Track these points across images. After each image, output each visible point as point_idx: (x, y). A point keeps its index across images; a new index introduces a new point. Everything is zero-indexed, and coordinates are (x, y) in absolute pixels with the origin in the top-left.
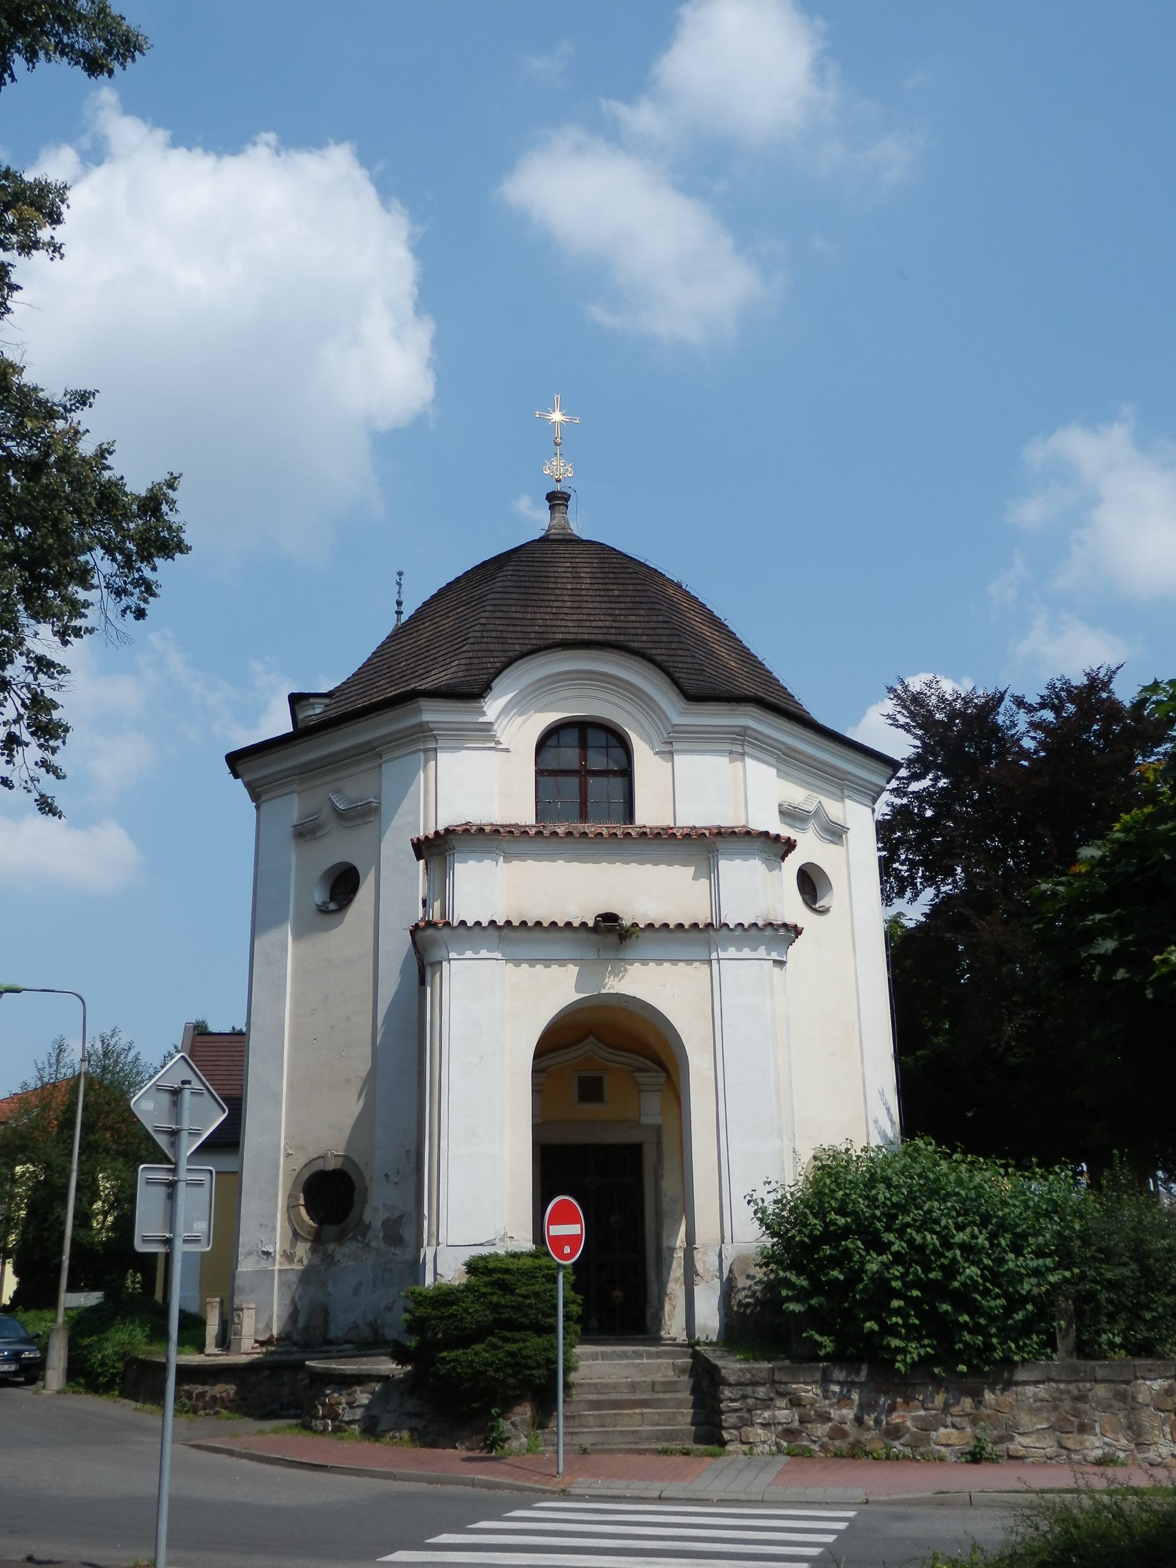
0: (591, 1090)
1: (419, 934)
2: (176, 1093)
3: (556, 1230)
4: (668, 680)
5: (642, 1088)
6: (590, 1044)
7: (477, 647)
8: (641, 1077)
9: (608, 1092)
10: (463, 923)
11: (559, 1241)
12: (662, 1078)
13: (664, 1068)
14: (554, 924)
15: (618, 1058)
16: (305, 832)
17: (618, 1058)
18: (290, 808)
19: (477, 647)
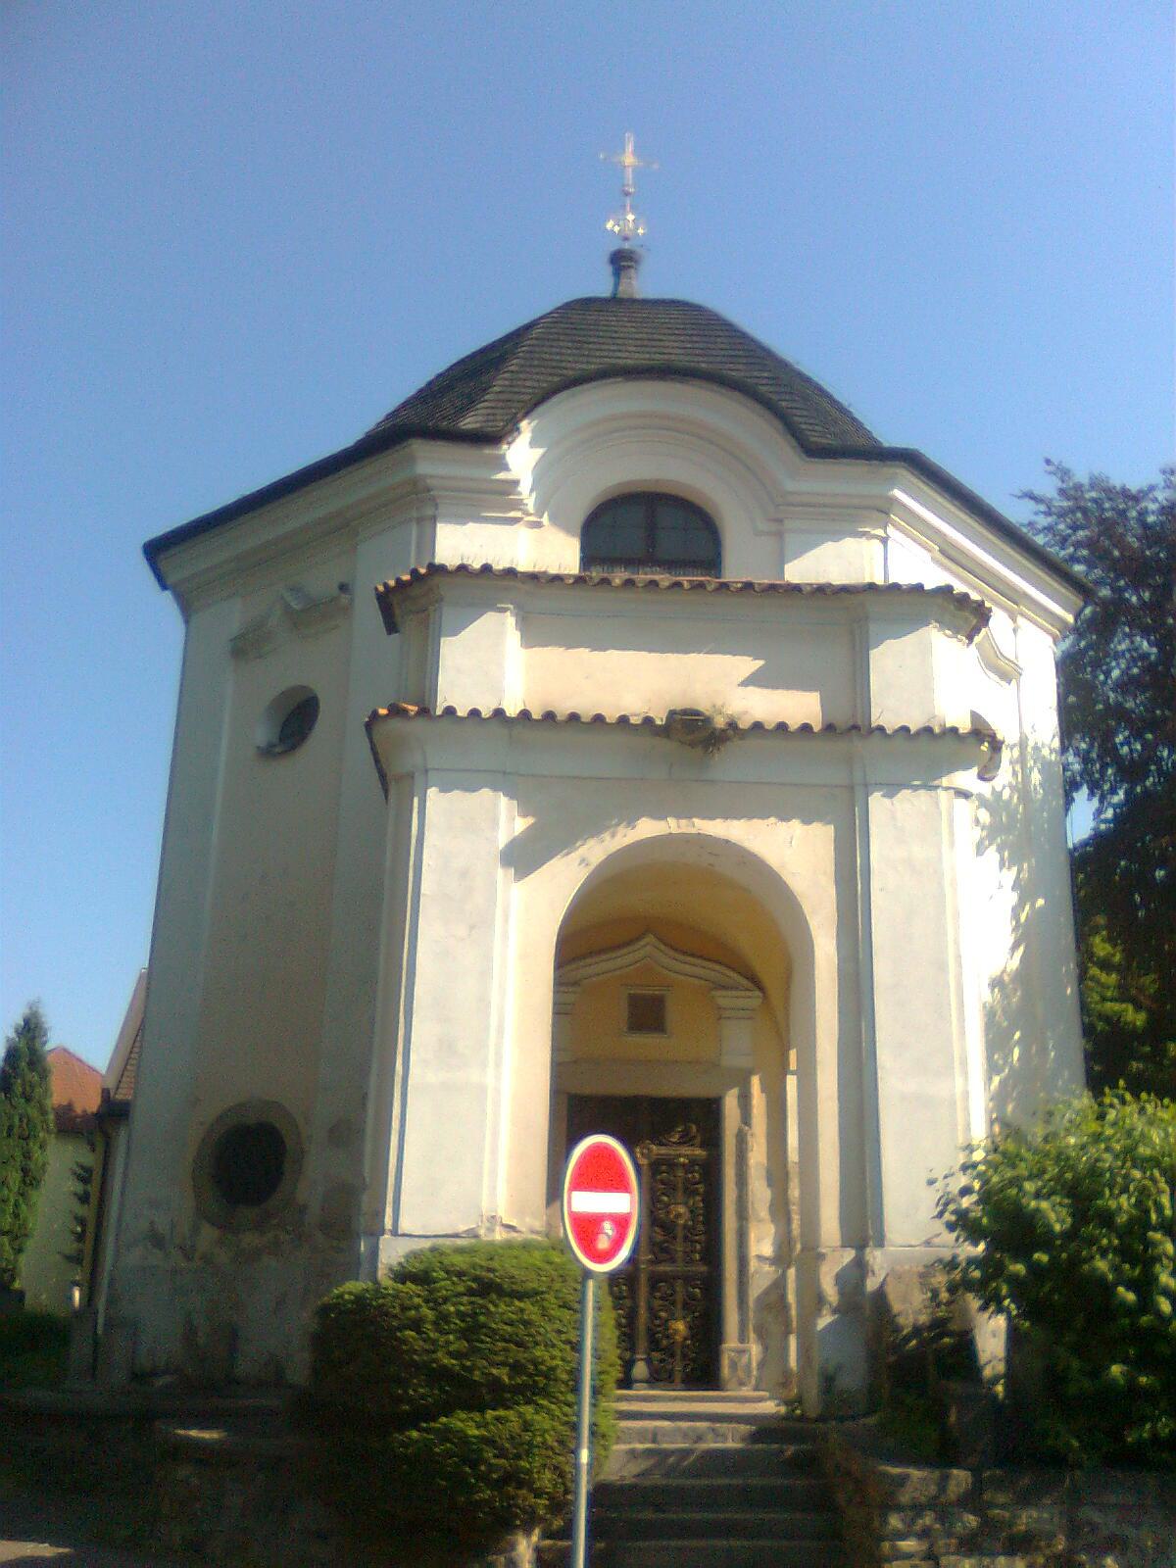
0: (647, 1014)
1: (380, 730)
2: (344, 1329)
3: (586, 1202)
4: (780, 426)
5: (727, 1014)
6: (647, 948)
7: (501, 397)
8: (724, 999)
9: (673, 1014)
10: (450, 711)
11: (586, 1226)
12: (754, 999)
13: (757, 983)
14: (599, 719)
15: (688, 968)
16: (246, 647)
17: (688, 968)
18: (231, 616)
19: (501, 397)
